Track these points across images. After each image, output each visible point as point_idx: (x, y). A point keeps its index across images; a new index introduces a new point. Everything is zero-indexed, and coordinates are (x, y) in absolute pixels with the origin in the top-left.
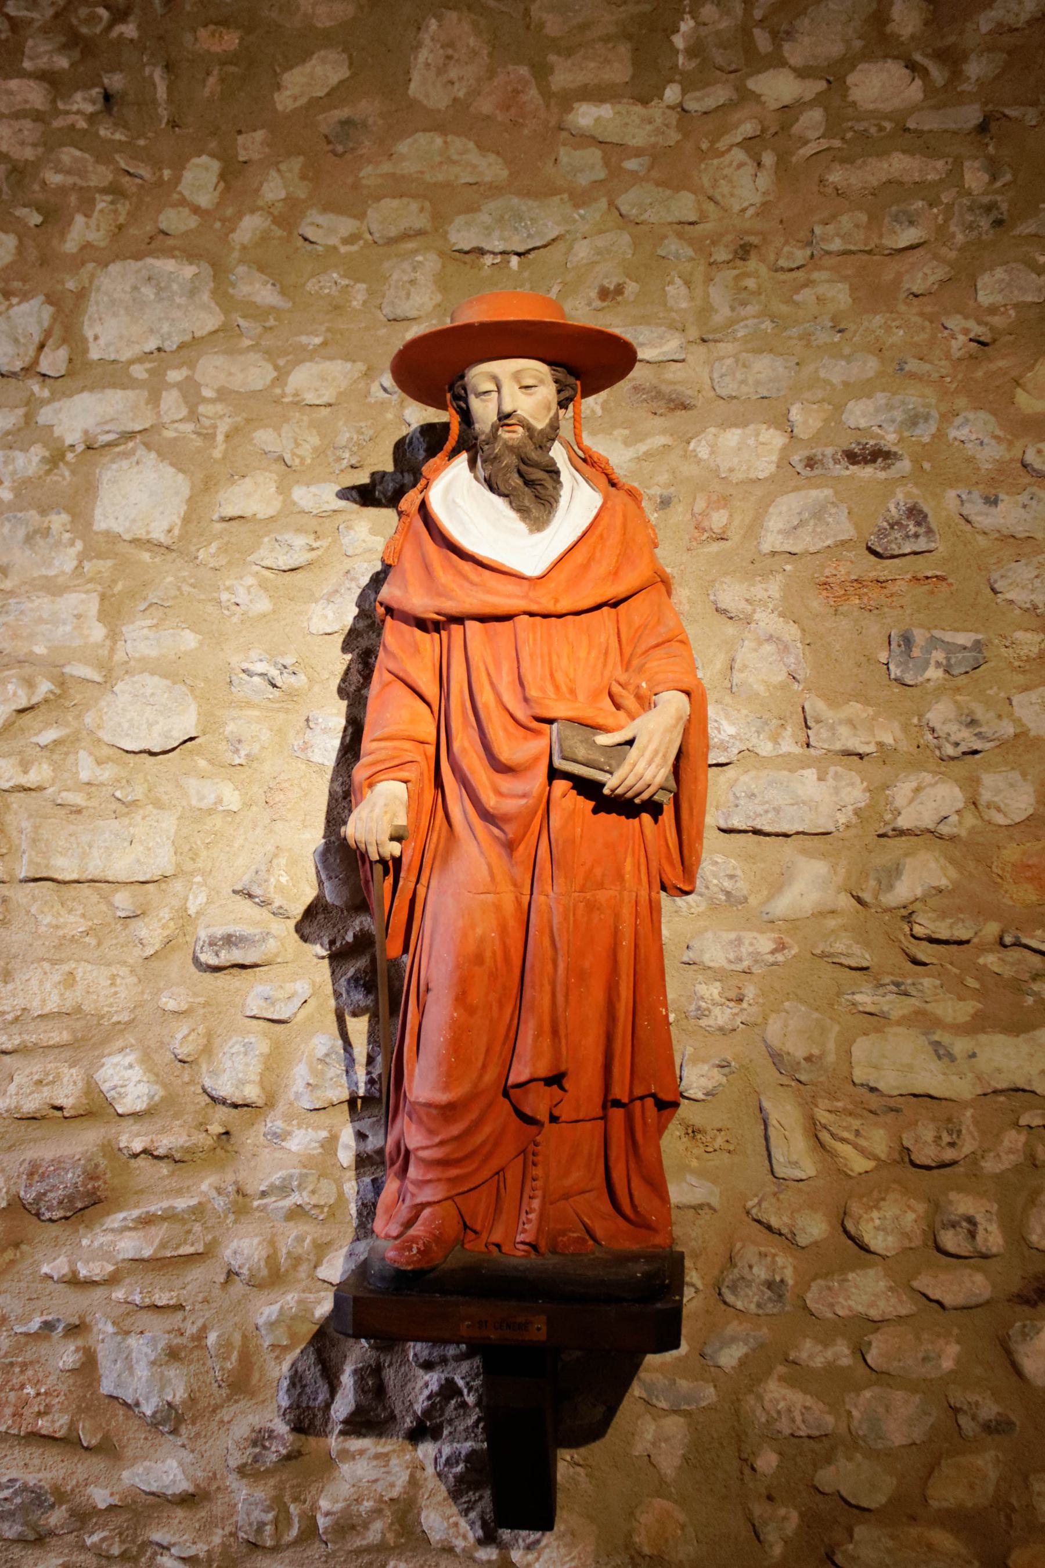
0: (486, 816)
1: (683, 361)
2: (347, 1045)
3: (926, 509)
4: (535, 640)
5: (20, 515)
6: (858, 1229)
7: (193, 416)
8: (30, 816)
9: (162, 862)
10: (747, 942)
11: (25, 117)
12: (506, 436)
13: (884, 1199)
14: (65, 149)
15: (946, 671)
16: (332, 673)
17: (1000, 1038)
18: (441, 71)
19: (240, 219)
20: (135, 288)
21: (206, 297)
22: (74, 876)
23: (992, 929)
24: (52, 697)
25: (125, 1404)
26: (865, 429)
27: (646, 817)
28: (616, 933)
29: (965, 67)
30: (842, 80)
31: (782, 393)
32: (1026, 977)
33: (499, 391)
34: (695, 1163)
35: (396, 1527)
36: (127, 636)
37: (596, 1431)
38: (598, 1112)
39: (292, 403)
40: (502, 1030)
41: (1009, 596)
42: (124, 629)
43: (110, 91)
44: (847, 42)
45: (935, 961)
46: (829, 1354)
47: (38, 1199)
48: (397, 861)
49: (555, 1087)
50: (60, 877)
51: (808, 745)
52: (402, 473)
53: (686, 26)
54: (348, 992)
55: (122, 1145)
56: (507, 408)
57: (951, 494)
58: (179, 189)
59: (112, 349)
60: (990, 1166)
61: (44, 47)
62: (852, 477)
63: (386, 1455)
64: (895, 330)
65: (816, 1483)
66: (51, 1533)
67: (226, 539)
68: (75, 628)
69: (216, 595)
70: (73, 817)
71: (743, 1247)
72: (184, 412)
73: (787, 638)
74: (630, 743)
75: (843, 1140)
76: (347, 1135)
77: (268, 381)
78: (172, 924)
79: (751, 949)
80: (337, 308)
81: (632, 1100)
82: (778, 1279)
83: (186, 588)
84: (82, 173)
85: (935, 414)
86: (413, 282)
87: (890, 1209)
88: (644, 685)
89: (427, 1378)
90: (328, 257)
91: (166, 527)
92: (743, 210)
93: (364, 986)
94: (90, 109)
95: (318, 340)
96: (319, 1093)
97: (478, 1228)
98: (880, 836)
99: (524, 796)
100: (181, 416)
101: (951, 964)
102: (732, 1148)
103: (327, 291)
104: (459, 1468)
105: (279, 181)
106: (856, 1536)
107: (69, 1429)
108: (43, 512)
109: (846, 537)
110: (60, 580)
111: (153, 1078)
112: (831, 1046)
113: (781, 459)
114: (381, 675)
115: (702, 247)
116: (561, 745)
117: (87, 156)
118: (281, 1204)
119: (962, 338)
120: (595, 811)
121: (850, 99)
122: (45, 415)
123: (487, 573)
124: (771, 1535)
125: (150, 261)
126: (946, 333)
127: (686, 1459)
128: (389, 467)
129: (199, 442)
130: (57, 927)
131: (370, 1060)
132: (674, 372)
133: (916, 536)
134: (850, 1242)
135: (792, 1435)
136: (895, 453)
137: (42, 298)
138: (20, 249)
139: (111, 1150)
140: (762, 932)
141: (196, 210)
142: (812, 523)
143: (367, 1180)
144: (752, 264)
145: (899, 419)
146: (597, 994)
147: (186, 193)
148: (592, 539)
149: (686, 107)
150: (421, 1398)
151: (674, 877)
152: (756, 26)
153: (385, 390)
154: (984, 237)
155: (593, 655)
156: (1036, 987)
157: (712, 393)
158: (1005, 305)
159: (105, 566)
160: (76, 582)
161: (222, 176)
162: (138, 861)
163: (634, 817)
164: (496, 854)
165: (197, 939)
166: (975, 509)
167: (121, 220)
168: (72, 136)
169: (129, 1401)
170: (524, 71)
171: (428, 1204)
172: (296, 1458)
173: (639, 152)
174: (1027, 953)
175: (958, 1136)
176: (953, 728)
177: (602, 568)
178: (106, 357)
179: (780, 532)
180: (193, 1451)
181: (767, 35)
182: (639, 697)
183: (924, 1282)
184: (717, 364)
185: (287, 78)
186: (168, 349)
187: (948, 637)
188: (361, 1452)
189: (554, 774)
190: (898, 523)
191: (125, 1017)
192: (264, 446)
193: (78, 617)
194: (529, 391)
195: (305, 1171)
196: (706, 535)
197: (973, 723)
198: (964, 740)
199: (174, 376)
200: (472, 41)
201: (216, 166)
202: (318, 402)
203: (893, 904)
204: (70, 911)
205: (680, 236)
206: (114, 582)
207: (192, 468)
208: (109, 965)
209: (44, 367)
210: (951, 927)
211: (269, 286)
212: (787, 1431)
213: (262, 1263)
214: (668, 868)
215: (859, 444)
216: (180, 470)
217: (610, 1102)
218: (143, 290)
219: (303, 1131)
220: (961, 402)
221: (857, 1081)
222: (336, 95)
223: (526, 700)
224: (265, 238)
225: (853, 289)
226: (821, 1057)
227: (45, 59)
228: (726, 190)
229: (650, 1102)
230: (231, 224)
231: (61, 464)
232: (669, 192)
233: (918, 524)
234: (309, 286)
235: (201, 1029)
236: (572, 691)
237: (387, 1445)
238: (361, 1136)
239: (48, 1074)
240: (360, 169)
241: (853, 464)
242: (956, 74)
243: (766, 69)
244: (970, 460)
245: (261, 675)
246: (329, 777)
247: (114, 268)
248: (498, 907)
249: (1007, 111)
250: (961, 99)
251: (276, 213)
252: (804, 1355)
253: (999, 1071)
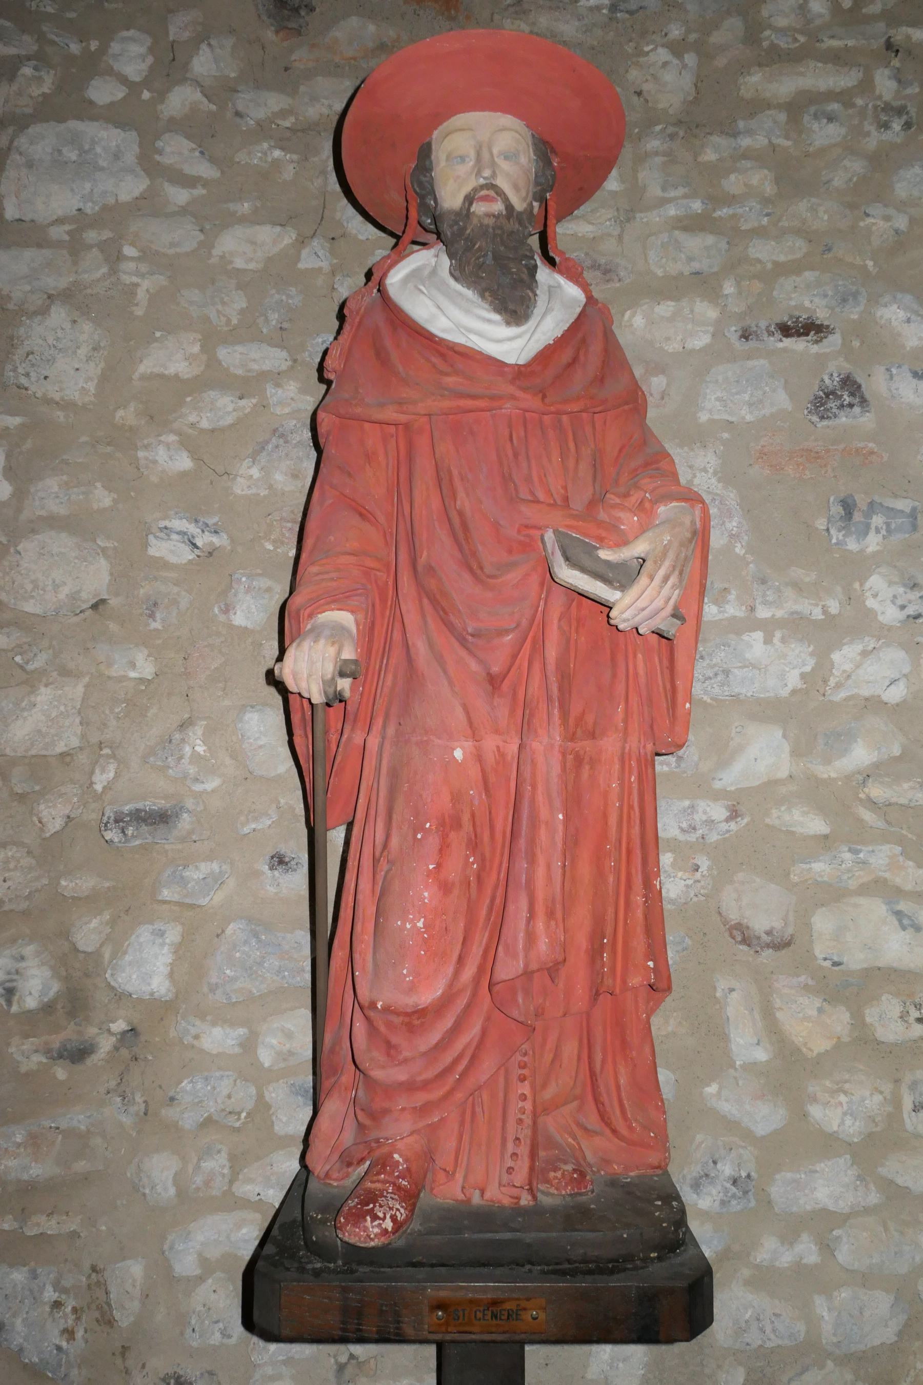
9: (69, 740)
10: (700, 810)
79: (704, 818)
190: (833, 393)
233: (852, 394)
245: (179, 533)
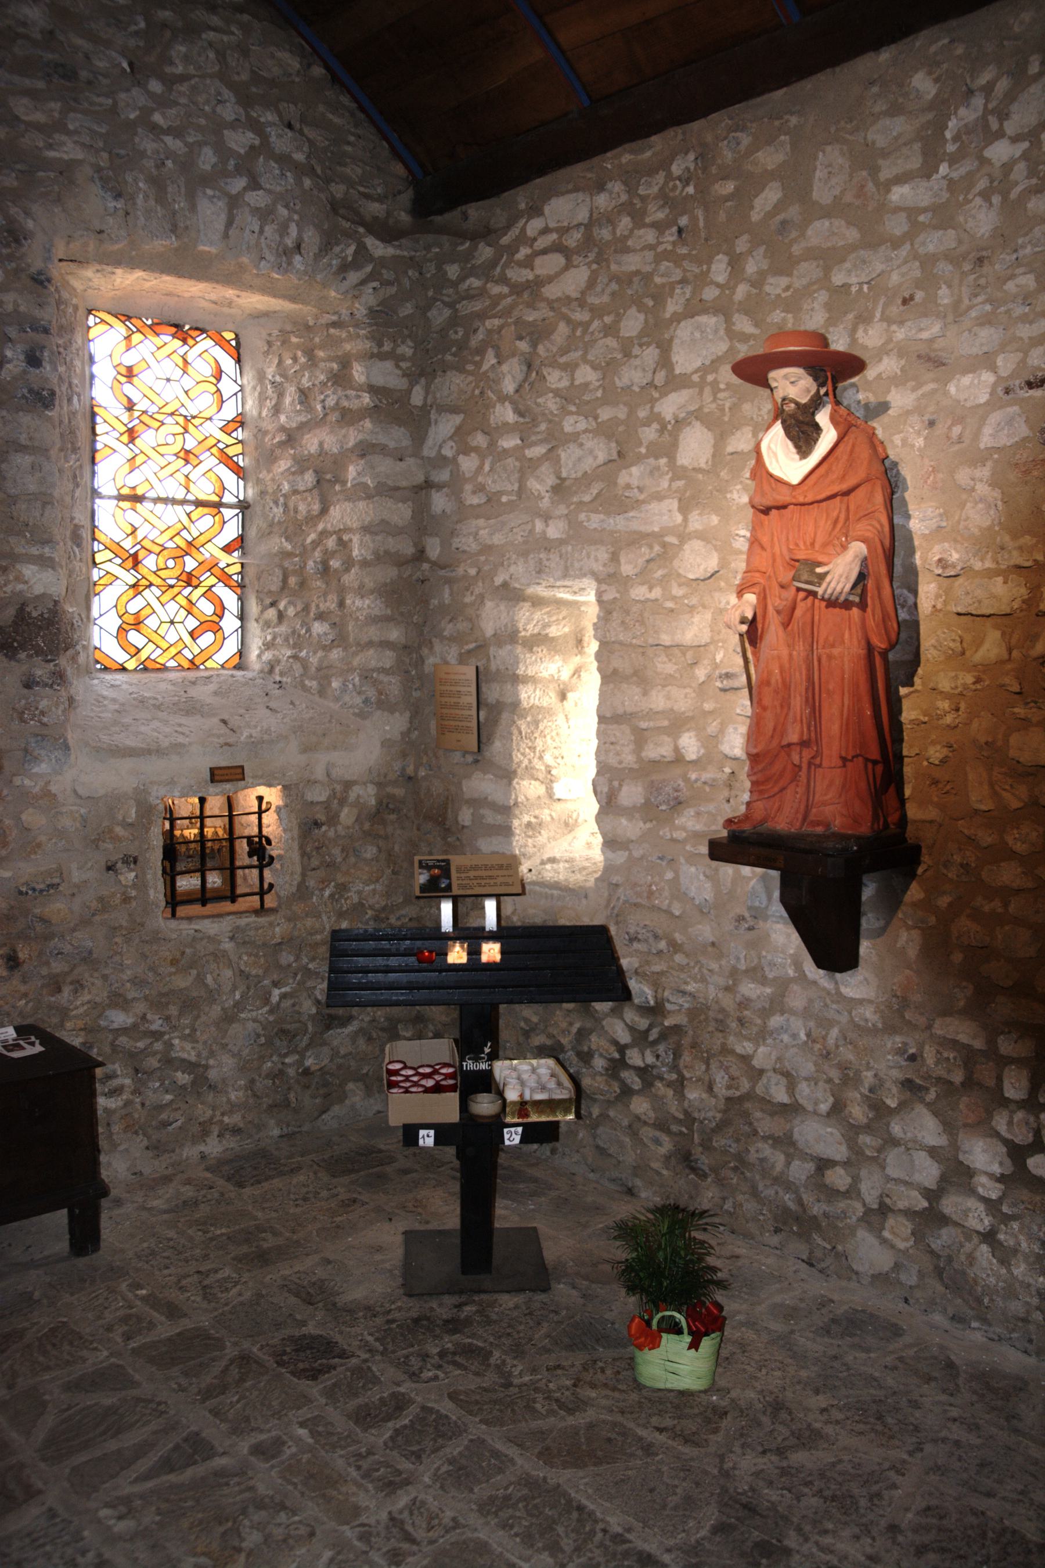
9: (706, 637)
34: (936, 799)
86: (812, 310)
94: (671, 239)
112: (1000, 736)
144: (986, 269)
148: (831, 459)
159: (680, 483)
161: (729, 264)
168: (666, 255)
191: (690, 714)
200: (840, 161)
222: (779, 207)
224: (749, 295)
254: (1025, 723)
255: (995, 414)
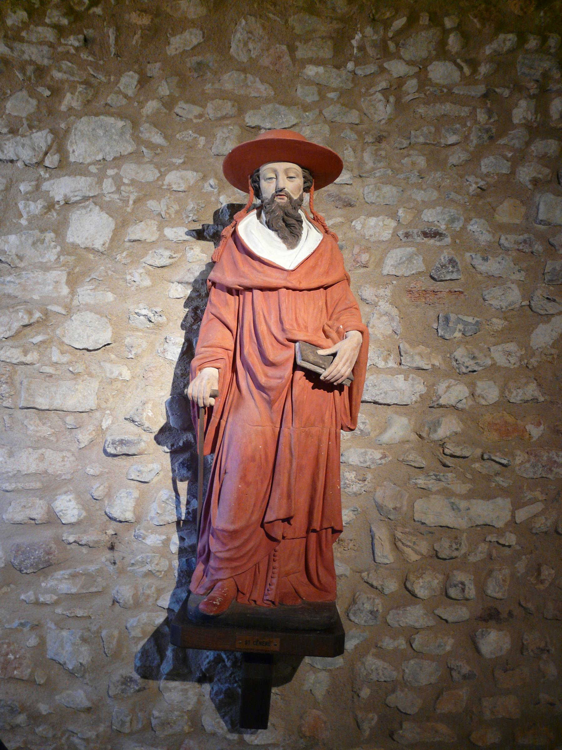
0: (259, 387)
1: (351, 184)
2: (177, 495)
3: (457, 260)
4: (289, 301)
5: (30, 232)
6: (412, 587)
7: (118, 191)
8: (26, 377)
9: (91, 403)
10: (369, 453)
11: (44, 44)
12: (279, 201)
13: (424, 573)
14: (63, 62)
15: (463, 334)
16: (179, 317)
17: (481, 502)
18: (246, 44)
19: (147, 102)
20: (94, 130)
21: (128, 136)
22: (47, 407)
23: (478, 452)
24: (41, 320)
25: (59, 663)
26: (431, 222)
27: (337, 392)
28: (319, 448)
29: (479, 69)
30: (425, 67)
31: (395, 203)
32: (493, 474)
33: (277, 178)
35: (190, 723)
36: (80, 293)
37: (287, 679)
38: (304, 534)
39: (167, 189)
40: (262, 495)
41: (491, 302)
42: (78, 290)
43: (87, 37)
44: (429, 51)
45: (453, 465)
46: (396, 643)
47: (20, 564)
48: (211, 408)
49: (286, 523)
50: (39, 408)
51: (400, 364)
52: (217, 225)
53: (358, 36)
54: (179, 469)
55: (64, 539)
56: (281, 186)
57: (468, 255)
58: (118, 85)
59: (81, 157)
60: (472, 559)
61: (56, 13)
62: (424, 243)
63: (186, 689)
64: (446, 180)
65: (387, 702)
66: (18, 726)
67: (131, 250)
68: (54, 288)
69: (124, 276)
70: (47, 379)
71: (360, 594)
72: (114, 189)
73: (393, 314)
74: (334, 355)
75: (407, 546)
76: (175, 538)
77: (156, 178)
78: (94, 433)
79: (371, 457)
80: (191, 147)
81: (321, 530)
82: (375, 610)
83: (110, 273)
84: (72, 74)
85: (462, 218)
87: (427, 578)
88: (341, 327)
89: (208, 653)
90: (187, 124)
91: (102, 243)
92: (380, 121)
93: (187, 467)
94: (76, 44)
95: (181, 161)
96: (162, 518)
97: (245, 592)
98: (430, 407)
99: (280, 378)
100: (112, 190)
101: (460, 467)
102: (356, 548)
103: (186, 139)
104: (221, 697)
105: (166, 87)
106: (404, 727)
107: (30, 675)
108: (42, 231)
109: (421, 270)
110: (49, 264)
111: (81, 507)
112: (405, 503)
113: (393, 232)
114: (208, 315)
115: (361, 136)
116: (301, 353)
117: (74, 66)
118: (141, 569)
119: (474, 186)
120: (313, 388)
121: (429, 77)
122: (46, 186)
123: (266, 267)
124: (366, 726)
125: (102, 117)
126: (468, 183)
127: (328, 692)
128: (211, 222)
129: (120, 204)
130: (37, 431)
131: (188, 503)
132: (346, 189)
133: (452, 272)
134: (407, 592)
135: (378, 681)
136: (445, 234)
137: (48, 130)
138: (38, 107)
139: (59, 541)
140: (376, 449)
141: (126, 96)
142: (407, 262)
143: (184, 560)
144: (383, 145)
145: (447, 219)
146: (307, 477)
147: (122, 88)
149: (356, 72)
150: (205, 663)
151: (348, 423)
152: (389, 40)
153: (211, 186)
154: (485, 143)
155: (315, 311)
156: (497, 479)
157: (363, 201)
158: (493, 174)
159: (71, 259)
160: (56, 266)
161: (139, 82)
162: (79, 401)
163: (331, 392)
164: (262, 406)
165: (106, 441)
166: (478, 261)
167: (89, 98)
168: (66, 56)
169: (61, 662)
170: (284, 47)
171: (221, 580)
172: (142, 690)
173: (335, 90)
174: (493, 463)
175: (460, 545)
176: (466, 359)
177: (321, 270)
178: (78, 161)
179: (392, 265)
180: (91, 686)
181: (394, 44)
182: (338, 332)
183: (440, 611)
184: (366, 188)
185: (173, 40)
186: (108, 160)
187: (465, 318)
188: (175, 688)
189: (296, 367)
190: (445, 266)
191: (69, 477)
192: (152, 208)
193: (56, 282)
194: (291, 180)
195: (153, 554)
196: (359, 264)
197: (474, 358)
198: (470, 365)
199: (110, 172)
201: (137, 76)
202: (179, 190)
203: (436, 439)
204: (44, 424)
205: (352, 129)
206: (75, 267)
207: (116, 215)
208: (62, 451)
209: (47, 163)
210: (461, 450)
211: (159, 134)
212: (375, 679)
213: (131, 598)
214: (344, 418)
215: (428, 229)
216: (111, 216)
217: (310, 530)
218: (97, 131)
219: (154, 535)
220: (472, 214)
221: (416, 519)
223: (283, 330)
224: (157, 113)
225: (428, 161)
226: (400, 508)
227: (56, 19)
228: (373, 111)
229: (330, 531)
230: (142, 104)
231: (52, 210)
232: (347, 109)
233: (453, 267)
234: (178, 136)
235: (106, 484)
236: (306, 327)
237: (188, 685)
238: (182, 539)
239: (28, 503)
240: (205, 85)
241: (425, 237)
242: (475, 71)
243: (394, 59)
244: (476, 240)
246: (174, 366)
247: (85, 119)
248: (263, 433)
249: (497, 90)
250: (476, 82)
251: (164, 101)
252: (385, 644)
253: (479, 516)
254: (425, 492)
255: (398, 250)
